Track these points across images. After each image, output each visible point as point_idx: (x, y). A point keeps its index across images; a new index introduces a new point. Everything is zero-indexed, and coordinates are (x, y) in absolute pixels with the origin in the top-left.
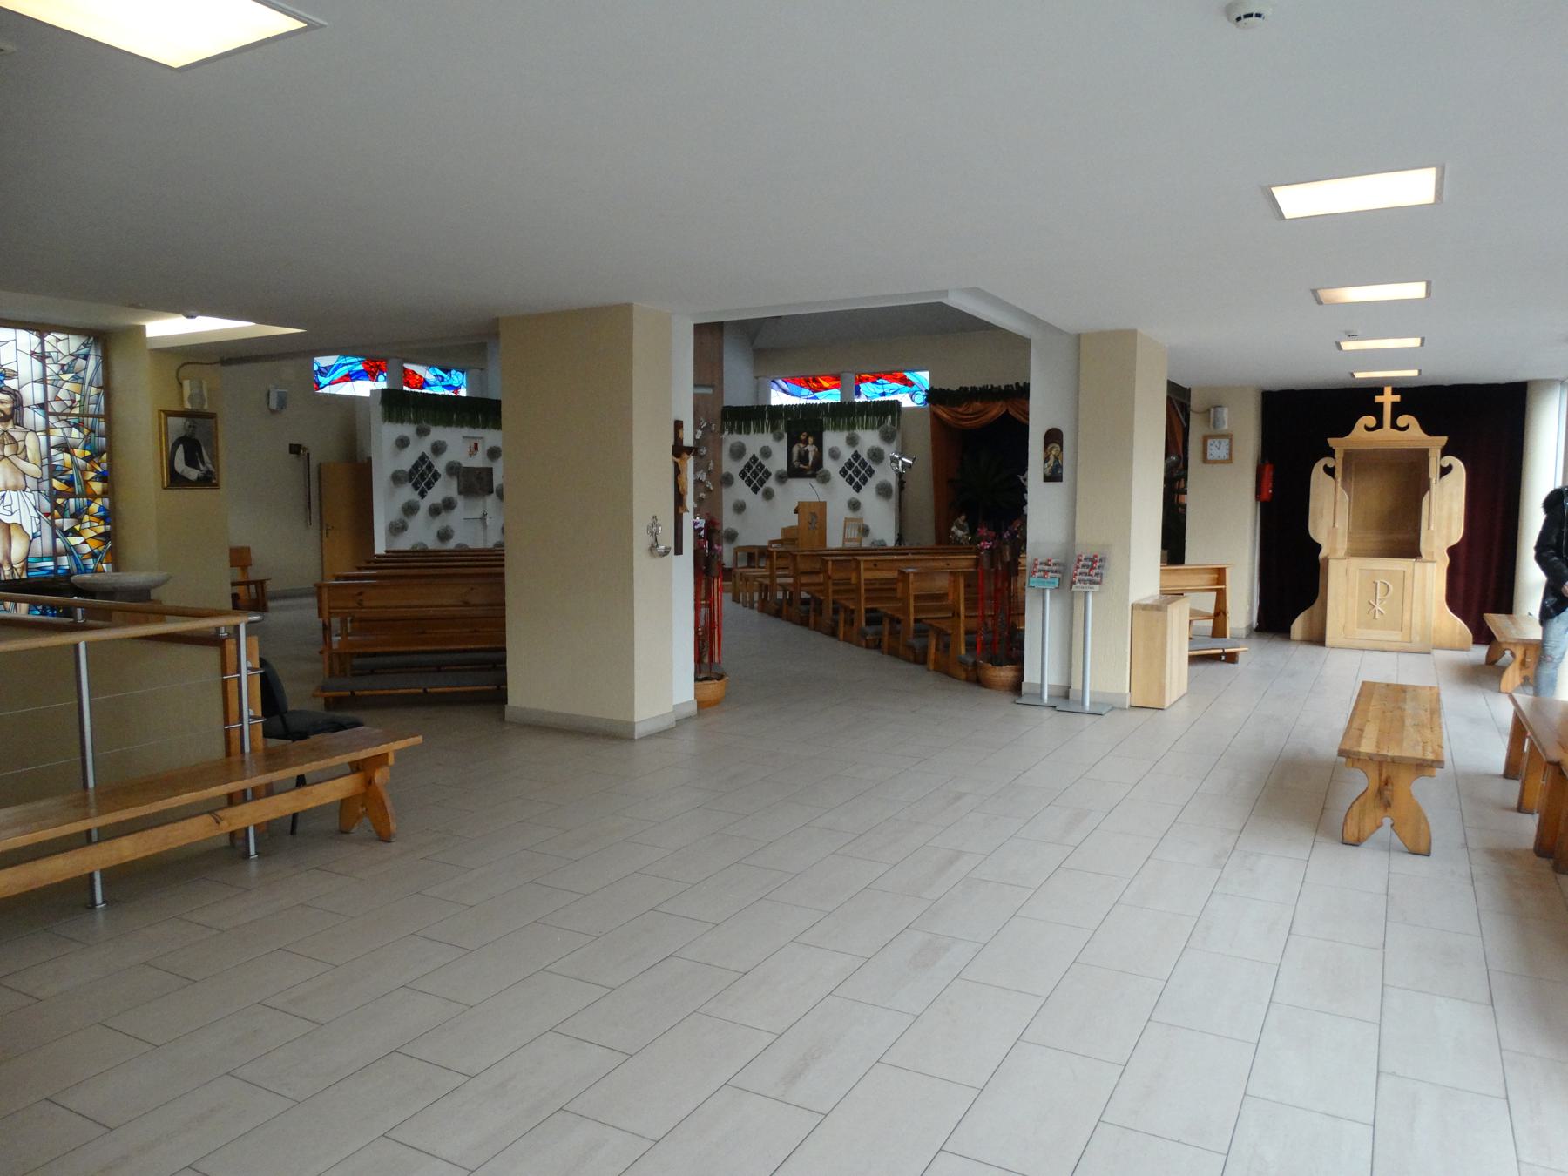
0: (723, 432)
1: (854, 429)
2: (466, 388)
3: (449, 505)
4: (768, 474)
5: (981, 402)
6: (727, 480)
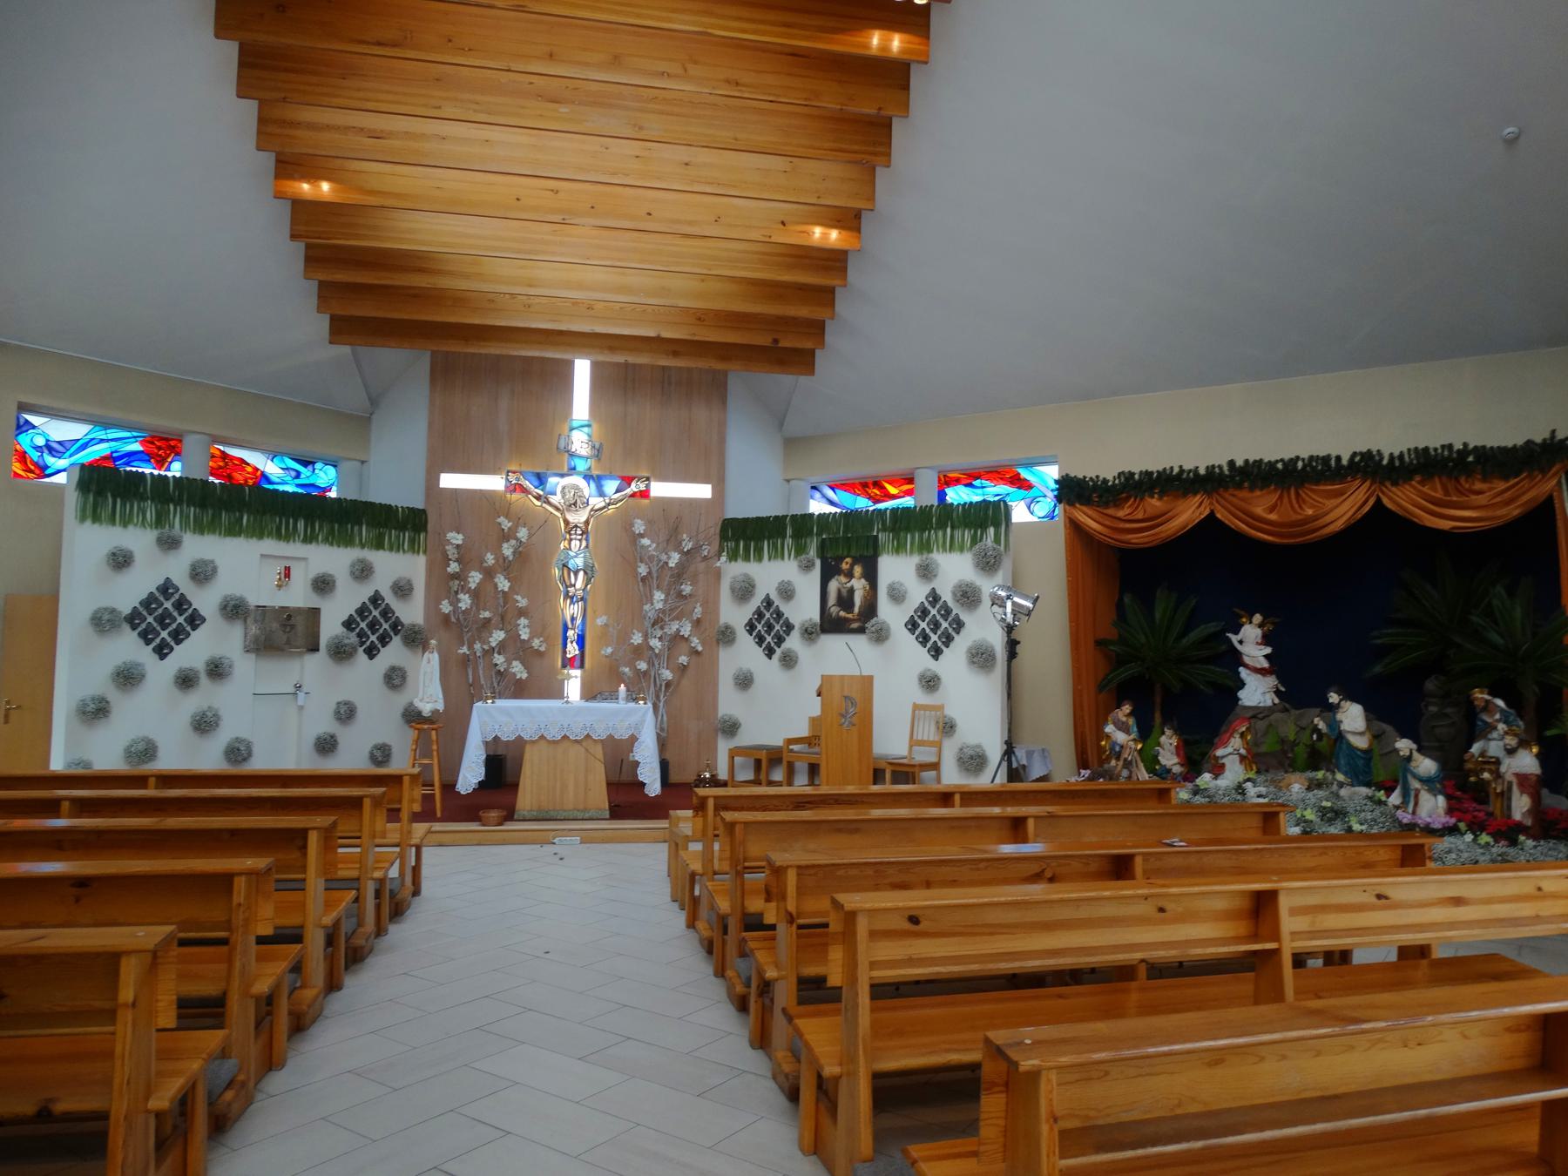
0: (719, 556)
1: (930, 551)
2: (337, 486)
3: (217, 670)
4: (789, 627)
5: (1160, 499)
6: (726, 636)
